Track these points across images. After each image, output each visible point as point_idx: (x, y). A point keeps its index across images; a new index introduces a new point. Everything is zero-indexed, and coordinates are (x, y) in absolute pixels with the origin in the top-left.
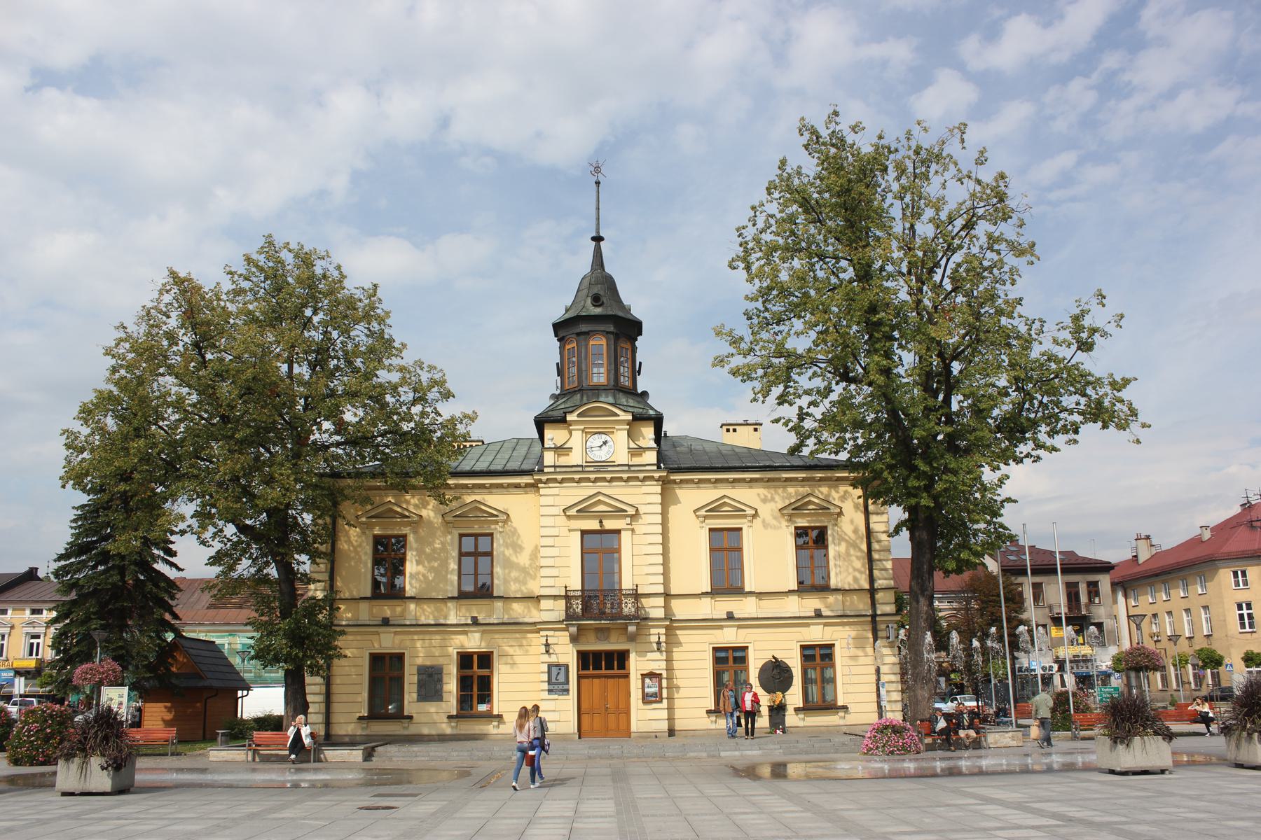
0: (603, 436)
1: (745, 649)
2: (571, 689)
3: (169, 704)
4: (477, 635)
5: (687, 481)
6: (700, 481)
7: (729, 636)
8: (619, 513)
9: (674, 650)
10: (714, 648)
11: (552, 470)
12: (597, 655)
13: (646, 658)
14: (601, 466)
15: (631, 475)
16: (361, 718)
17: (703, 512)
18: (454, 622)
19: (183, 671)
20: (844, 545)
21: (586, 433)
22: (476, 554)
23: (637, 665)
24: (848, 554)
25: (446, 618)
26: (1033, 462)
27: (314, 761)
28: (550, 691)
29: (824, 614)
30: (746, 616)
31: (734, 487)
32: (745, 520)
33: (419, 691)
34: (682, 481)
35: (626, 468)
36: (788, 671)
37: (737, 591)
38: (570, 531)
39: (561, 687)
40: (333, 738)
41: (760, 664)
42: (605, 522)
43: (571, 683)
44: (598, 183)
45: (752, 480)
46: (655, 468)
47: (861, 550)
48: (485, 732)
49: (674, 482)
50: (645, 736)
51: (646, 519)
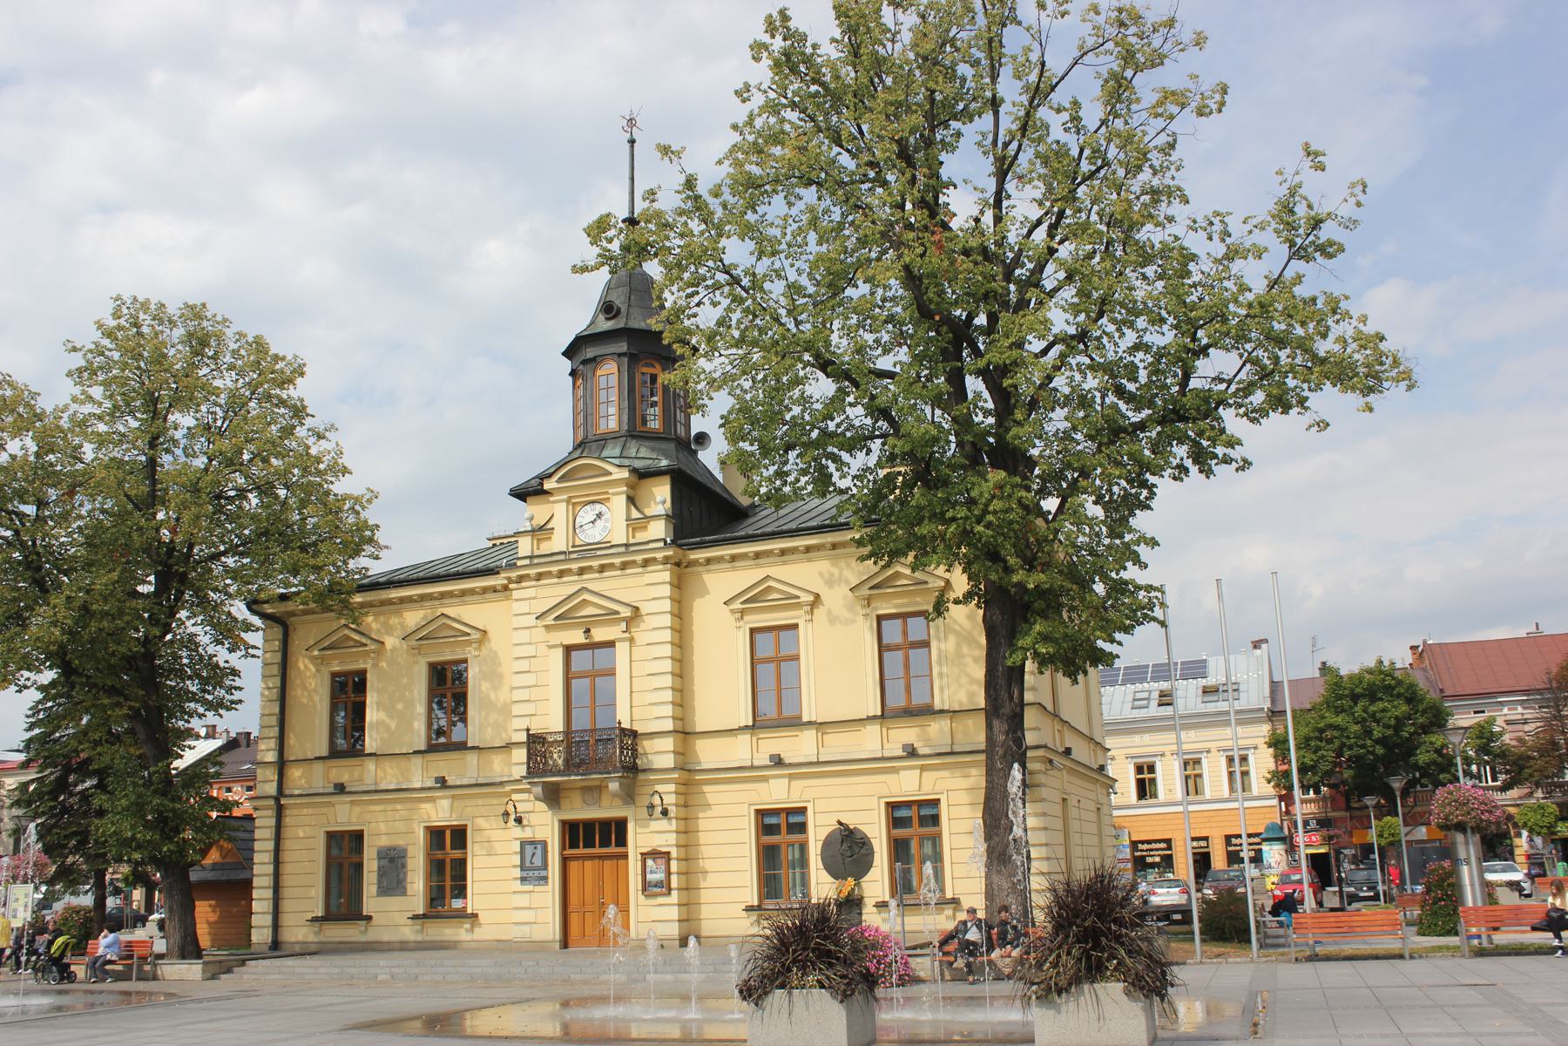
0: (598, 506)
1: (802, 811)
2: (550, 876)
3: (213, 902)
4: (445, 803)
5: (720, 560)
6: (733, 558)
7: (778, 793)
8: (610, 617)
9: (701, 815)
10: (758, 811)
11: (527, 562)
12: (589, 825)
13: (648, 830)
14: (589, 550)
15: (628, 558)
16: (315, 920)
17: (737, 605)
18: (418, 785)
19: (228, 860)
20: (952, 639)
21: (574, 504)
22: (778, 660)
23: (643, 836)
24: (959, 654)
25: (409, 781)
26: (1237, 470)
27: (139, 979)
28: (523, 879)
29: (921, 751)
30: (802, 760)
31: (784, 563)
32: (801, 612)
33: (379, 882)
34: (709, 561)
35: (622, 549)
36: (864, 844)
37: (795, 723)
38: (550, 647)
39: (536, 873)
40: (283, 946)
41: (823, 834)
42: (594, 631)
43: (550, 868)
44: (632, 142)
45: (808, 549)
46: (662, 544)
47: (979, 645)
48: (456, 938)
49: (694, 563)
50: (504, 948)
51: (649, 622)
